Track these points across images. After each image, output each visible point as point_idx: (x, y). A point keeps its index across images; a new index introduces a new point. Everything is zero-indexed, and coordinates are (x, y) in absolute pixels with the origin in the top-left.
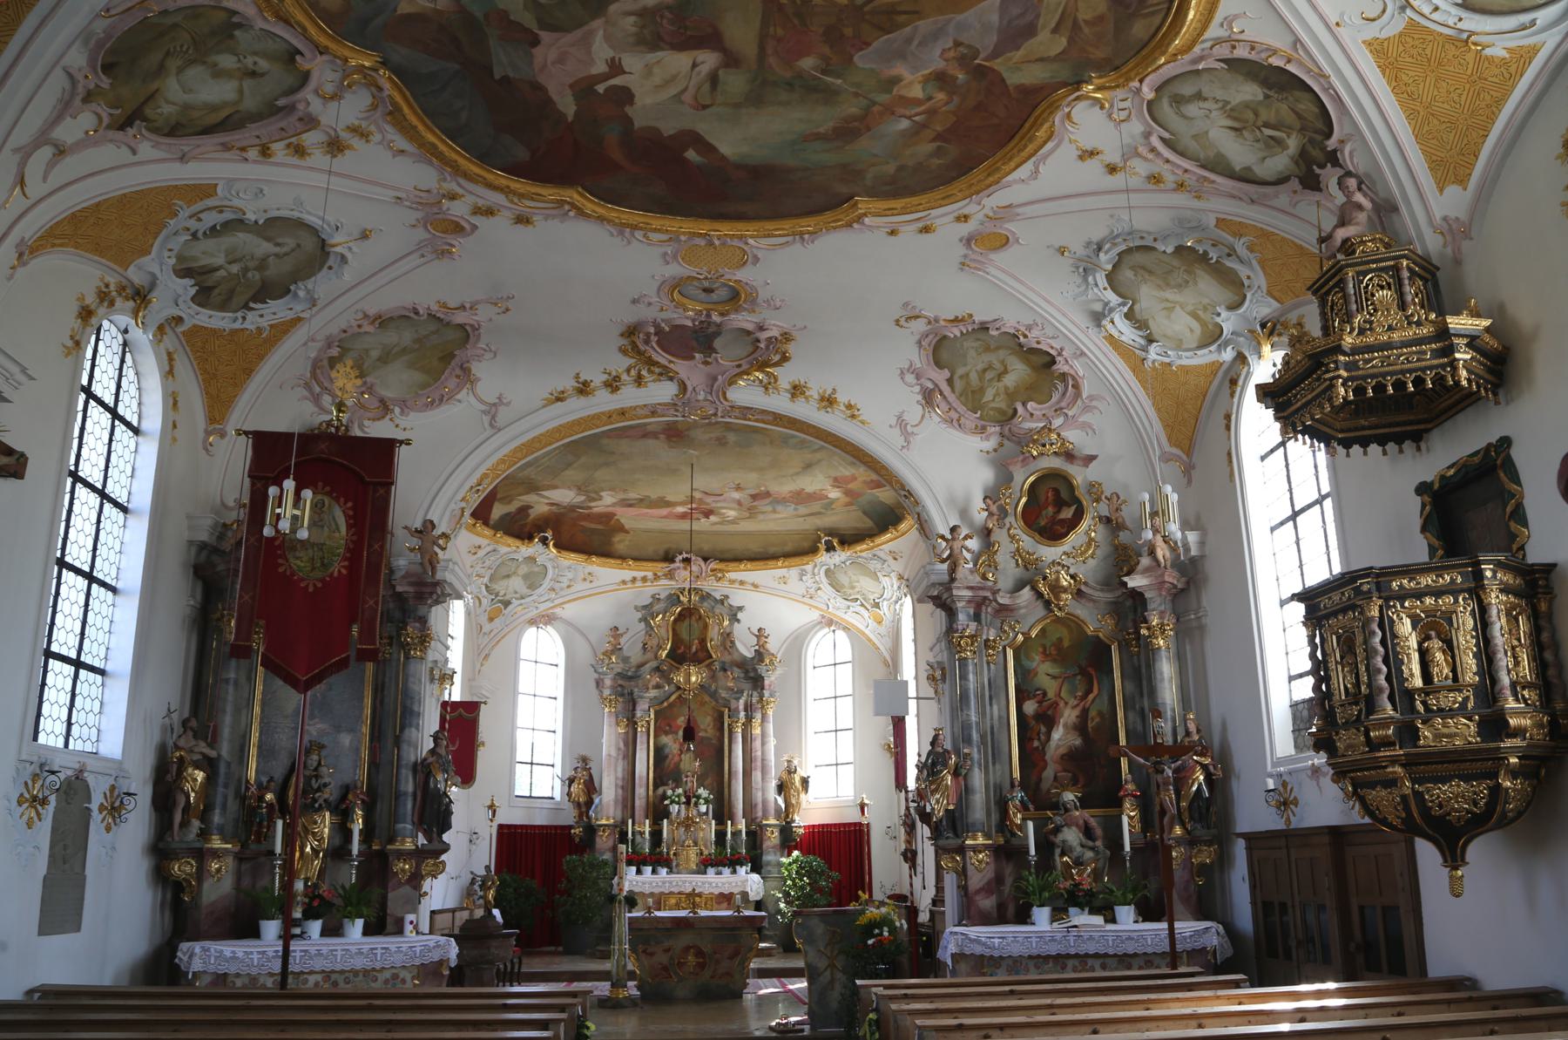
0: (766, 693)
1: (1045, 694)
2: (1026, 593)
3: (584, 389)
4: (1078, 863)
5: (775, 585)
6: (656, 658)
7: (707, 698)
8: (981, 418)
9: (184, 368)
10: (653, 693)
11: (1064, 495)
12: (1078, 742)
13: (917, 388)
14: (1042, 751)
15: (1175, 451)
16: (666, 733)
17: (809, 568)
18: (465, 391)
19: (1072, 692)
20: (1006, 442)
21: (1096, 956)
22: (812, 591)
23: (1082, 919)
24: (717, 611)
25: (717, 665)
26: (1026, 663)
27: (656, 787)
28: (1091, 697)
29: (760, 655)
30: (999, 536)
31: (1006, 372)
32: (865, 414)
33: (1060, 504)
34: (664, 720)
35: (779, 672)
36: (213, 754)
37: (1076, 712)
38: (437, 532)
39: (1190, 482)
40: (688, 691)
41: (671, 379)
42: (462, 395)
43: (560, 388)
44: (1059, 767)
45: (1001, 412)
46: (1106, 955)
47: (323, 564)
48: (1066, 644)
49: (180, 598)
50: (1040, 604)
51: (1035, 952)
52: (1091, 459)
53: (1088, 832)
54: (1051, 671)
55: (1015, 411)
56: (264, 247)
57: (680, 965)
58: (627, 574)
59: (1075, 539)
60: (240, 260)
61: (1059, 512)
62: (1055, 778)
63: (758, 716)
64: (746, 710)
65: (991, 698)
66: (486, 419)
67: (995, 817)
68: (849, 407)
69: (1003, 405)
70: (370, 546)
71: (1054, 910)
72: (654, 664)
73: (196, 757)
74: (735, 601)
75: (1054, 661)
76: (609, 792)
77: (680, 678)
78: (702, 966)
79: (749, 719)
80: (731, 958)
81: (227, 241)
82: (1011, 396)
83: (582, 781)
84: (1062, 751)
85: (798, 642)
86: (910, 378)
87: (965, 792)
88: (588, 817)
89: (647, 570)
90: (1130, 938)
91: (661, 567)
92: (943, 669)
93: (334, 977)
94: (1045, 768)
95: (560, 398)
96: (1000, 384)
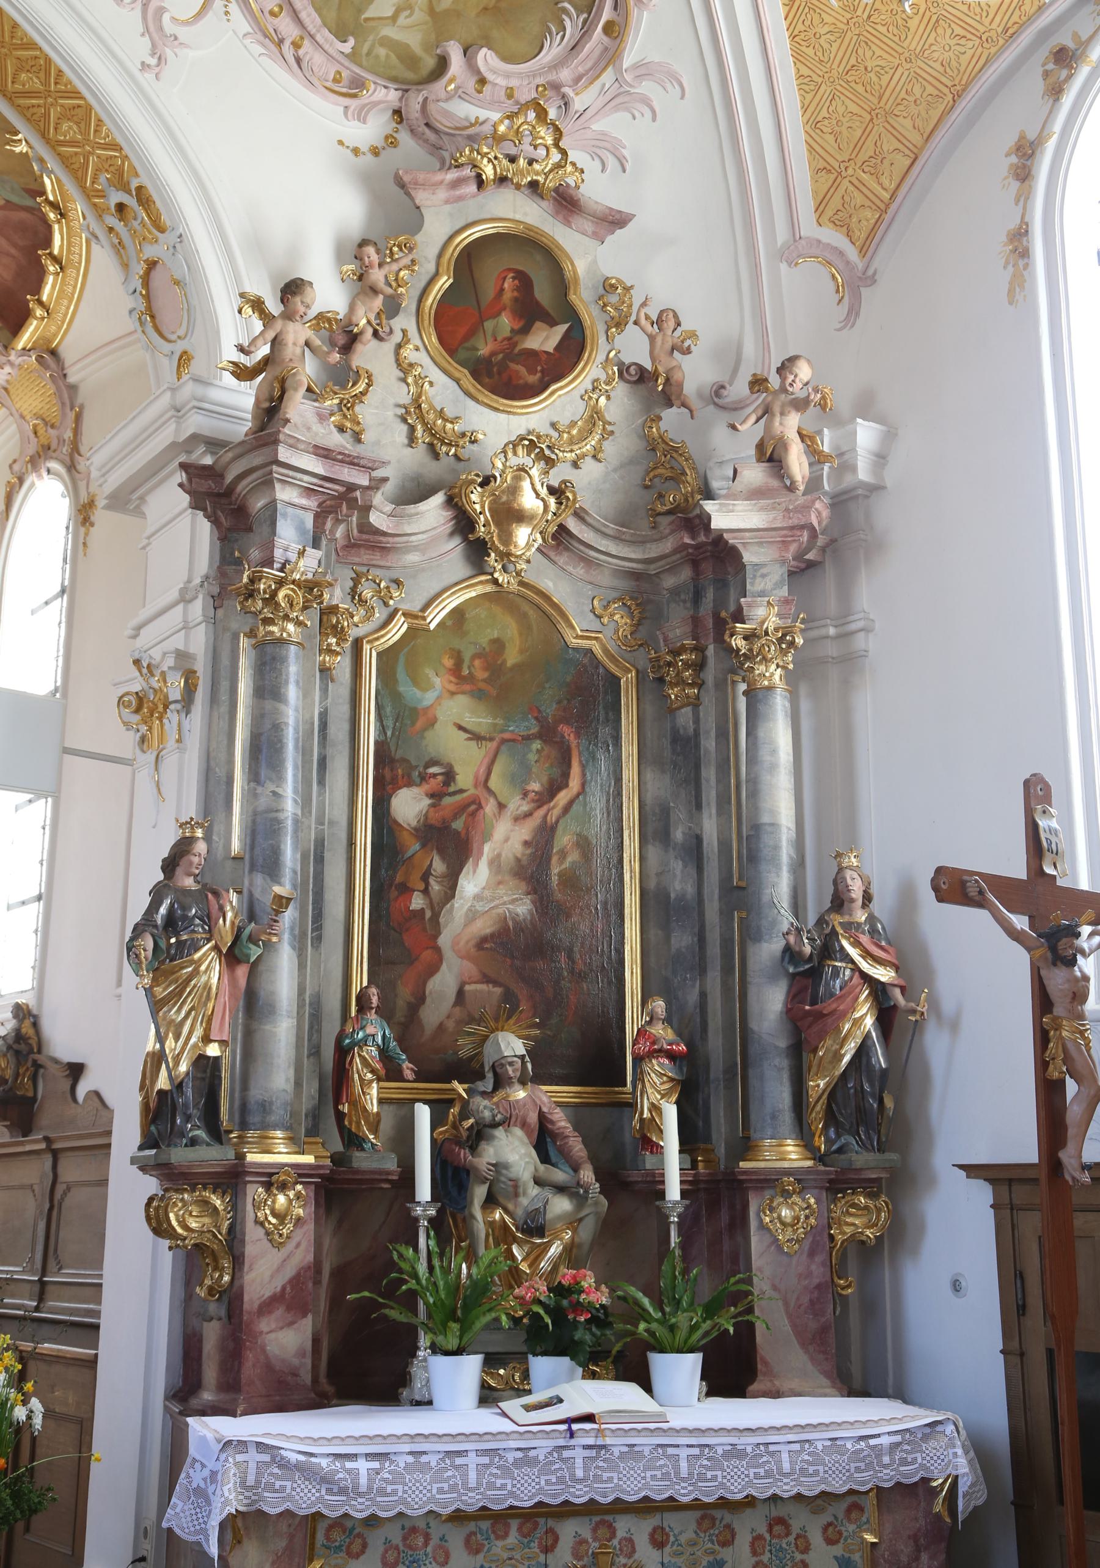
1: (449, 776)
2: (433, 512)
4: (535, 1227)
11: (543, 293)
12: (523, 908)
14: (430, 925)
15: (831, 236)
19: (518, 781)
20: (404, 137)
21: (645, 1507)
23: (573, 1389)
26: (407, 689)
28: (563, 797)
30: (371, 356)
33: (530, 313)
37: (525, 831)
39: (854, 312)
44: (470, 969)
45: (409, 59)
46: (671, 1505)
48: (512, 657)
50: (454, 546)
51: (472, 1501)
52: (615, 221)
53: (544, 1141)
55: (443, 64)
59: (559, 405)
61: (525, 330)
62: (460, 993)
69: (413, 40)
71: (491, 1361)
75: (479, 695)
84: (483, 926)
87: (253, 1005)
90: (735, 1453)
92: (190, 676)
94: (433, 968)
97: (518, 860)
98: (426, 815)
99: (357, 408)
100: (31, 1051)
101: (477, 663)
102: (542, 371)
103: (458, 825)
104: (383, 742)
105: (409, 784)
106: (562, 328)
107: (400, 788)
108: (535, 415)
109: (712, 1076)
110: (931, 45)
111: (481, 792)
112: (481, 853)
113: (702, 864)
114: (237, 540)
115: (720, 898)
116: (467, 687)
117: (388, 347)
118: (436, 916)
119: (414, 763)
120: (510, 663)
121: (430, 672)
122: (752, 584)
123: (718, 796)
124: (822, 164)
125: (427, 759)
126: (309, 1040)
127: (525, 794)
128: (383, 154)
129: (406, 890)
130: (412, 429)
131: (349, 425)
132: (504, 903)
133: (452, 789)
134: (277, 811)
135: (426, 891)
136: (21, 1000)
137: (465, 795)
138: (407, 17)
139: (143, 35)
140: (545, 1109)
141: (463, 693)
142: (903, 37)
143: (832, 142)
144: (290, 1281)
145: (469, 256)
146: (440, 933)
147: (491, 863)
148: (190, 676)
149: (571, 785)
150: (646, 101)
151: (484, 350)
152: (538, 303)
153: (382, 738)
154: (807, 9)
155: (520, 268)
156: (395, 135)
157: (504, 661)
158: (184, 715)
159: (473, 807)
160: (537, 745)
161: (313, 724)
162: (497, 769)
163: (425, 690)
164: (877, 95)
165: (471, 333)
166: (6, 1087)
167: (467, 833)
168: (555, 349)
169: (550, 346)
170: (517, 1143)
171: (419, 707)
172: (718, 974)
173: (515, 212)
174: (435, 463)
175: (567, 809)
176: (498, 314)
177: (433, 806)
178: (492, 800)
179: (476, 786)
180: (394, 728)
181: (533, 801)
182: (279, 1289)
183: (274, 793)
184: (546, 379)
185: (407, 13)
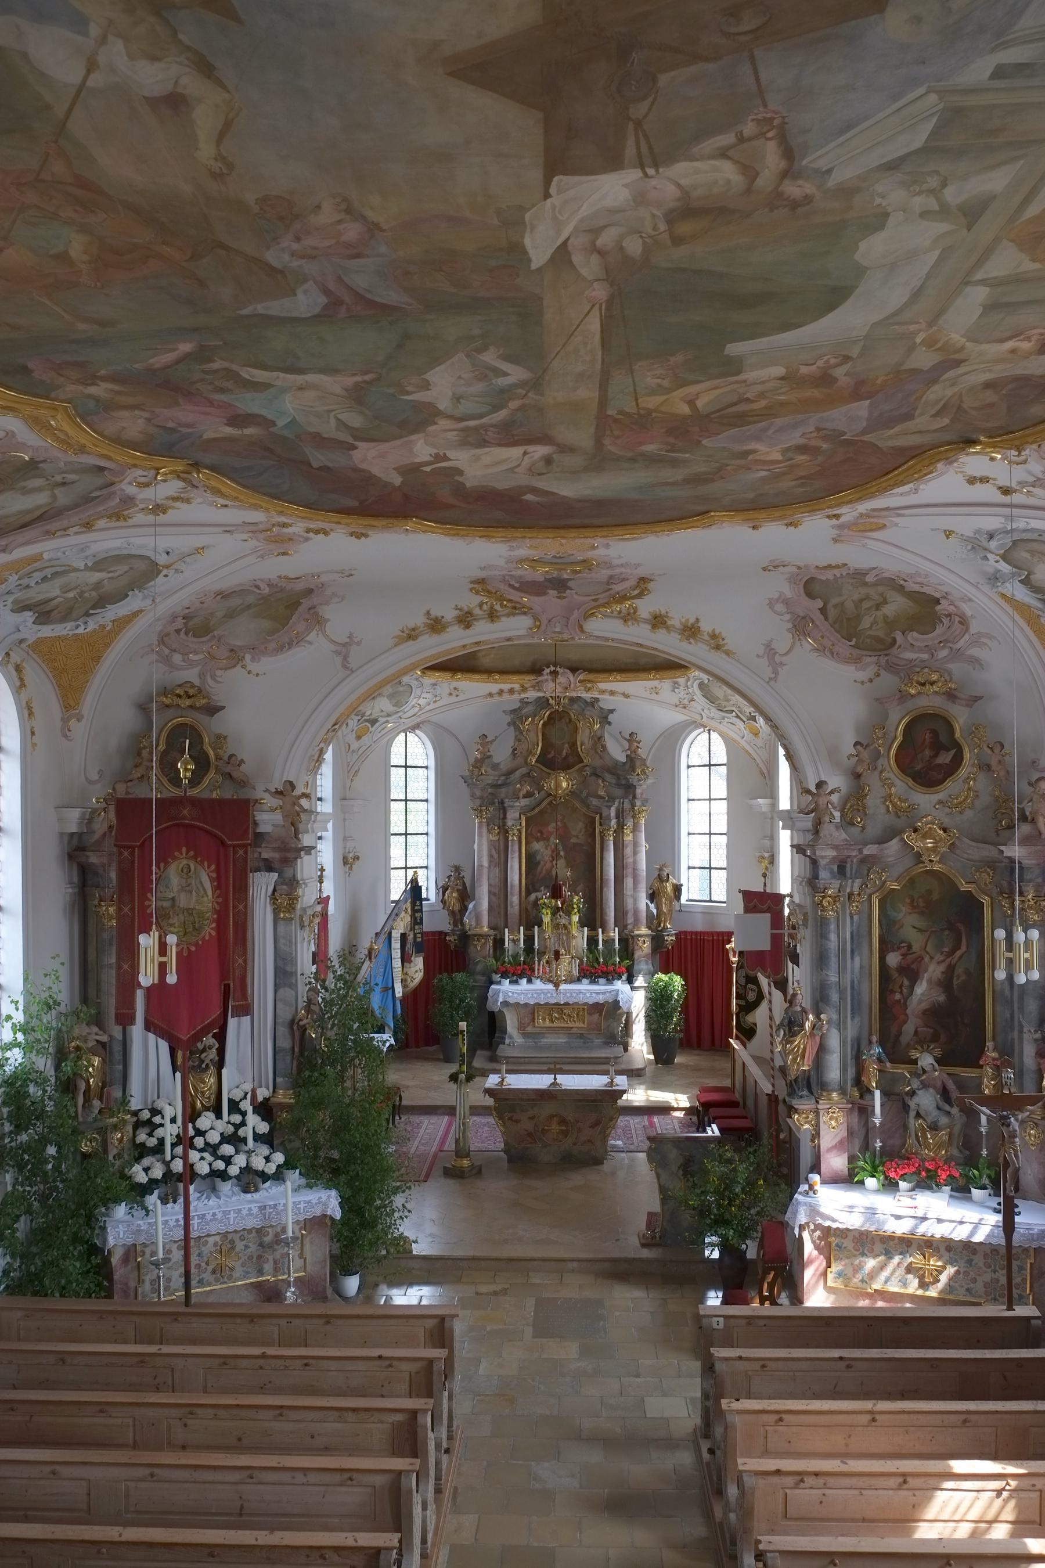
0: (638, 803)
1: (910, 947)
3: (436, 625)
5: (647, 695)
6: (526, 763)
7: (578, 805)
9: (34, 673)
10: (524, 802)
11: (944, 738)
12: (942, 998)
13: (787, 617)
16: (538, 840)
17: (682, 680)
18: (314, 632)
20: (882, 672)
22: (686, 701)
24: (587, 713)
25: (588, 771)
26: (892, 913)
27: (528, 893)
28: (958, 953)
29: (632, 760)
31: (885, 602)
32: (730, 643)
33: (938, 747)
34: (535, 824)
35: (649, 781)
36: (104, 1038)
37: (942, 968)
38: (298, 792)
40: (559, 797)
41: (525, 613)
42: (312, 636)
43: (411, 625)
45: (879, 640)
47: (194, 928)
49: (59, 890)
54: (917, 924)
55: (894, 640)
56: (97, 576)
57: (544, 1132)
58: (494, 688)
59: (952, 787)
60: (76, 588)
61: (936, 755)
62: (916, 1033)
63: (630, 823)
64: (617, 817)
65: (852, 952)
66: (339, 659)
67: (851, 1072)
68: (714, 636)
69: (881, 634)
70: (235, 907)
72: (524, 770)
73: (91, 1044)
74: (607, 706)
75: (922, 913)
76: (483, 901)
77: (549, 785)
78: (565, 1133)
79: (621, 826)
80: (594, 1126)
81: (59, 581)
82: (891, 624)
83: (458, 888)
84: (924, 1006)
85: (672, 740)
86: (780, 607)
87: (822, 1049)
88: (462, 924)
89: (513, 683)
91: (528, 679)
92: (805, 915)
93: (230, 1236)
94: (905, 1022)
95: (411, 635)
96: (879, 613)
103: (914, 966)
105: (893, 951)
106: (953, 752)
117: (876, 773)
118: (905, 1003)
129: (893, 992)
135: (901, 992)
151: (918, 767)
160: (947, 932)
169: (947, 761)
175: (960, 957)
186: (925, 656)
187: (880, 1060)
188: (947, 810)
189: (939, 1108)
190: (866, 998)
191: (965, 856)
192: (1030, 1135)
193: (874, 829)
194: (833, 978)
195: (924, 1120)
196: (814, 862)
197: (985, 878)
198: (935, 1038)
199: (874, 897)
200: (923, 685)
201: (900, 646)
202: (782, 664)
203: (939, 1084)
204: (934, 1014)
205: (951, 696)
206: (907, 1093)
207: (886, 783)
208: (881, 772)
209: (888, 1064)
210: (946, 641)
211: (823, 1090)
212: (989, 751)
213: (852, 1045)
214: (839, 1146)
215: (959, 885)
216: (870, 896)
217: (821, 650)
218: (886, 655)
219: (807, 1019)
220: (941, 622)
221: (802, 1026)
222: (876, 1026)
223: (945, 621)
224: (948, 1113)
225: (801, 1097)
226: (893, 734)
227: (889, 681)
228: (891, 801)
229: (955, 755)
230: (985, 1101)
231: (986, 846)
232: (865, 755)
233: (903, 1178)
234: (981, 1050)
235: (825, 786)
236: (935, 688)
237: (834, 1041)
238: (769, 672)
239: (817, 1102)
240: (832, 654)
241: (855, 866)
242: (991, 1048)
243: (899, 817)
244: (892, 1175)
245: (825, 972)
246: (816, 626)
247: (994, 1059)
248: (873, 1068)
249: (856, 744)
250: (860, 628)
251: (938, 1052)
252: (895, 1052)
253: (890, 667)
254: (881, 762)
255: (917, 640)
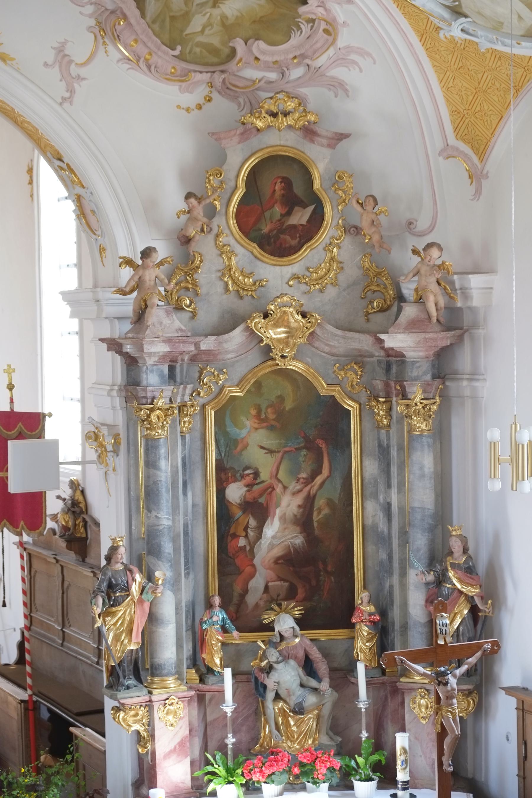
1: (256, 474)
8: (180, 57)
11: (298, 189)
12: (299, 540)
19: (294, 473)
20: (215, 95)
26: (231, 429)
28: (319, 480)
30: (205, 246)
33: (292, 202)
37: (299, 500)
39: (478, 193)
44: (271, 574)
45: (213, 51)
54: (266, 443)
55: (233, 52)
59: (311, 255)
61: (289, 213)
62: (267, 589)
69: (216, 41)
75: (271, 428)
82: (229, 29)
84: (277, 552)
87: (153, 618)
92: (116, 437)
94: (252, 576)
96: (216, 12)
97: (295, 516)
98: (245, 497)
99: (195, 276)
100: (82, 512)
101: (269, 410)
102: (300, 237)
103: (262, 500)
104: (220, 460)
105: (235, 481)
106: (311, 208)
107: (230, 484)
108: (297, 264)
109: (396, 628)
110: (499, 66)
111: (274, 482)
112: (275, 514)
113: (391, 518)
114: (133, 370)
115: (399, 539)
116: (265, 425)
117: (211, 238)
119: (237, 469)
120: (287, 408)
121: (244, 419)
122: (411, 372)
123: (398, 483)
124: (454, 109)
125: (244, 466)
126: (186, 623)
127: (298, 480)
128: (204, 107)
129: (235, 536)
130: (227, 283)
131: (190, 286)
132: (289, 539)
133: (258, 481)
134: (158, 526)
135: (246, 536)
136: (73, 478)
137: (265, 484)
138: (209, 30)
139: (61, 80)
140: (307, 649)
141: (262, 428)
142: (484, 60)
143: (458, 98)
144: (178, 743)
145: (254, 173)
146: (254, 557)
147: (281, 518)
148: (116, 437)
149: (323, 472)
150: (354, 62)
151: (265, 230)
152: (296, 196)
153: (219, 457)
154: (430, 40)
155: (284, 175)
156: (210, 95)
157: (284, 408)
158: (115, 457)
159: (270, 490)
160: (304, 452)
161: (177, 467)
162: (282, 468)
163: (241, 429)
164: (477, 82)
165: (258, 220)
166: (70, 533)
167: (267, 504)
168: (309, 221)
170: (290, 670)
171: (239, 438)
172: (398, 577)
173: (280, 140)
174: (240, 301)
176: (273, 206)
177: (248, 491)
178: (280, 485)
179: (271, 478)
180: (225, 452)
181: (303, 483)
182: (173, 748)
183: (156, 517)
184: (302, 241)
185: (210, 27)
186: (273, 76)
187: (224, 630)
188: (304, 287)
189: (302, 685)
190: (200, 549)
191: (327, 349)
192: (420, 706)
193: (208, 315)
194: (165, 519)
195: (285, 702)
196: (131, 363)
197: (352, 378)
198: (291, 595)
199: (208, 408)
200: (274, 115)
201: (241, 60)
202: (79, 78)
203: (301, 654)
204: (291, 563)
205: (309, 132)
206: (262, 670)
207: (222, 250)
208: (217, 236)
209: (235, 633)
210: (303, 56)
211: (153, 675)
212: (359, 208)
213: (187, 612)
214: (181, 748)
215: (319, 389)
216: (203, 407)
217: (141, 62)
218: (222, 72)
219: (134, 580)
220: (299, 28)
221: (127, 589)
222: (214, 584)
223: (305, 28)
224: (315, 690)
225: (128, 688)
226: (232, 184)
227: (223, 108)
228: (230, 276)
229: (314, 212)
230: (416, 657)
231: (356, 335)
232: (199, 211)
233: (269, 779)
234: (351, 607)
235: (154, 255)
236: (290, 120)
237: (168, 609)
238: (61, 90)
239: (150, 693)
240: (149, 67)
241: (185, 367)
242: (366, 600)
243: (241, 298)
244: (256, 777)
245: (154, 513)
246: (129, 25)
247: (370, 614)
248: (215, 638)
249: (189, 196)
250: (187, 32)
251: (298, 611)
252: (246, 619)
253: (228, 90)
254: (217, 221)
255: (264, 53)
